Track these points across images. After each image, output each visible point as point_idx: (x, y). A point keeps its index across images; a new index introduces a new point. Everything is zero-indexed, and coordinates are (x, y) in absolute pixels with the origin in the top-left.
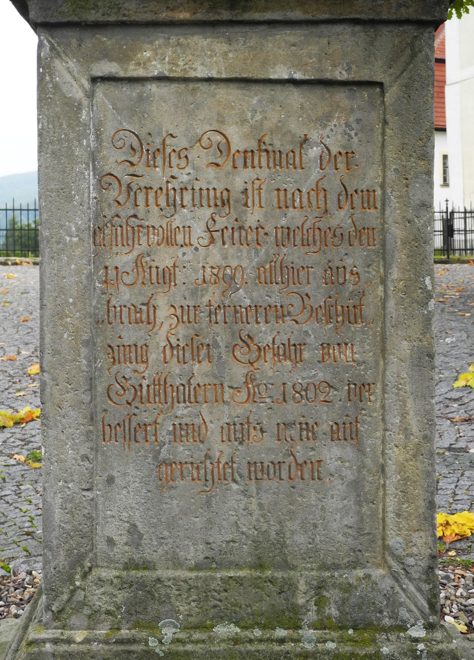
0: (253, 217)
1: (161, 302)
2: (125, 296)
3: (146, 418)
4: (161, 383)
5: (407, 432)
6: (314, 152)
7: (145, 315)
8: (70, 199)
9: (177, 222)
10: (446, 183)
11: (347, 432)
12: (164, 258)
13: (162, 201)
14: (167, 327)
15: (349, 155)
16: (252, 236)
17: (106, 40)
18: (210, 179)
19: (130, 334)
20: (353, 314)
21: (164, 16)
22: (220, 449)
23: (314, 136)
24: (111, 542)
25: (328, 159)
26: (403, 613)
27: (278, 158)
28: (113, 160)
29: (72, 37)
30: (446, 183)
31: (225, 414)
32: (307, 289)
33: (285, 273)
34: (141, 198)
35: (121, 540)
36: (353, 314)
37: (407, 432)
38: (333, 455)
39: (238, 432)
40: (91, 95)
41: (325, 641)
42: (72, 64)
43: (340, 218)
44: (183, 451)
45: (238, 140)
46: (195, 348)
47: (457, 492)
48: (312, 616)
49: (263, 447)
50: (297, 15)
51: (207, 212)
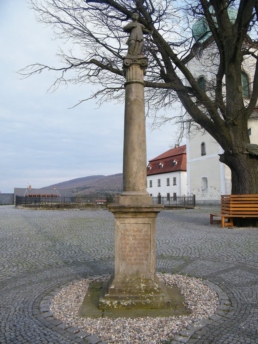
0: (137, 237)
1: (127, 246)
2: (123, 246)
3: (126, 258)
4: (127, 255)
5: (152, 260)
6: (143, 231)
7: (126, 248)
8: (118, 236)
9: (129, 238)
10: (151, 187)
11: (147, 260)
12: (128, 242)
13: (127, 236)
14: (128, 249)
15: (147, 231)
16: (137, 239)
17: (122, 219)
18: (133, 234)
19: (124, 250)
20: (147, 248)
21: (128, 217)
22: (133, 261)
23: (143, 229)
24: (122, 271)
25: (145, 232)
26: (152, 278)
27: (140, 231)
28: (122, 232)
29: (118, 219)
30: (151, 187)
31: (134, 258)
32: (142, 245)
33: (140, 243)
34: (125, 236)
35: (123, 270)
36: (147, 248)
37: (152, 260)
38: (145, 262)
39: (135, 260)
40: (120, 225)
41: (249, 180)
42: (118, 222)
43: (146, 237)
44: (129, 262)
45: (135, 229)
46: (130, 251)
47: (8, 319)
48: (142, 278)
49: (138, 261)
50: (142, 217)
51: (132, 237)
